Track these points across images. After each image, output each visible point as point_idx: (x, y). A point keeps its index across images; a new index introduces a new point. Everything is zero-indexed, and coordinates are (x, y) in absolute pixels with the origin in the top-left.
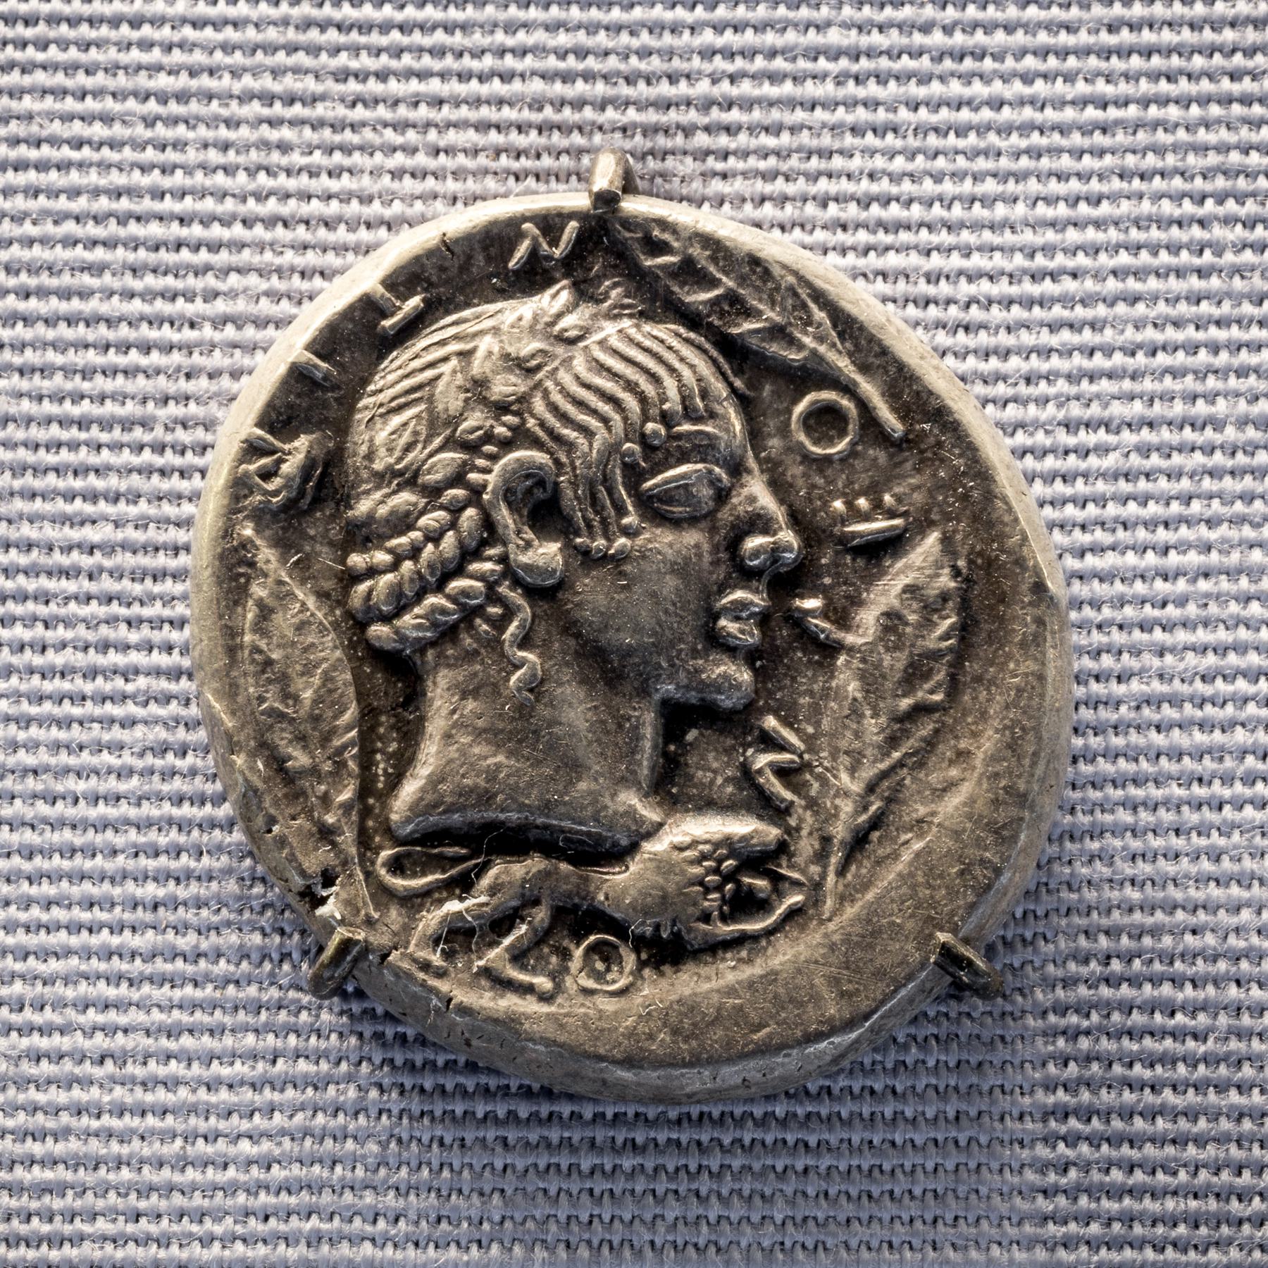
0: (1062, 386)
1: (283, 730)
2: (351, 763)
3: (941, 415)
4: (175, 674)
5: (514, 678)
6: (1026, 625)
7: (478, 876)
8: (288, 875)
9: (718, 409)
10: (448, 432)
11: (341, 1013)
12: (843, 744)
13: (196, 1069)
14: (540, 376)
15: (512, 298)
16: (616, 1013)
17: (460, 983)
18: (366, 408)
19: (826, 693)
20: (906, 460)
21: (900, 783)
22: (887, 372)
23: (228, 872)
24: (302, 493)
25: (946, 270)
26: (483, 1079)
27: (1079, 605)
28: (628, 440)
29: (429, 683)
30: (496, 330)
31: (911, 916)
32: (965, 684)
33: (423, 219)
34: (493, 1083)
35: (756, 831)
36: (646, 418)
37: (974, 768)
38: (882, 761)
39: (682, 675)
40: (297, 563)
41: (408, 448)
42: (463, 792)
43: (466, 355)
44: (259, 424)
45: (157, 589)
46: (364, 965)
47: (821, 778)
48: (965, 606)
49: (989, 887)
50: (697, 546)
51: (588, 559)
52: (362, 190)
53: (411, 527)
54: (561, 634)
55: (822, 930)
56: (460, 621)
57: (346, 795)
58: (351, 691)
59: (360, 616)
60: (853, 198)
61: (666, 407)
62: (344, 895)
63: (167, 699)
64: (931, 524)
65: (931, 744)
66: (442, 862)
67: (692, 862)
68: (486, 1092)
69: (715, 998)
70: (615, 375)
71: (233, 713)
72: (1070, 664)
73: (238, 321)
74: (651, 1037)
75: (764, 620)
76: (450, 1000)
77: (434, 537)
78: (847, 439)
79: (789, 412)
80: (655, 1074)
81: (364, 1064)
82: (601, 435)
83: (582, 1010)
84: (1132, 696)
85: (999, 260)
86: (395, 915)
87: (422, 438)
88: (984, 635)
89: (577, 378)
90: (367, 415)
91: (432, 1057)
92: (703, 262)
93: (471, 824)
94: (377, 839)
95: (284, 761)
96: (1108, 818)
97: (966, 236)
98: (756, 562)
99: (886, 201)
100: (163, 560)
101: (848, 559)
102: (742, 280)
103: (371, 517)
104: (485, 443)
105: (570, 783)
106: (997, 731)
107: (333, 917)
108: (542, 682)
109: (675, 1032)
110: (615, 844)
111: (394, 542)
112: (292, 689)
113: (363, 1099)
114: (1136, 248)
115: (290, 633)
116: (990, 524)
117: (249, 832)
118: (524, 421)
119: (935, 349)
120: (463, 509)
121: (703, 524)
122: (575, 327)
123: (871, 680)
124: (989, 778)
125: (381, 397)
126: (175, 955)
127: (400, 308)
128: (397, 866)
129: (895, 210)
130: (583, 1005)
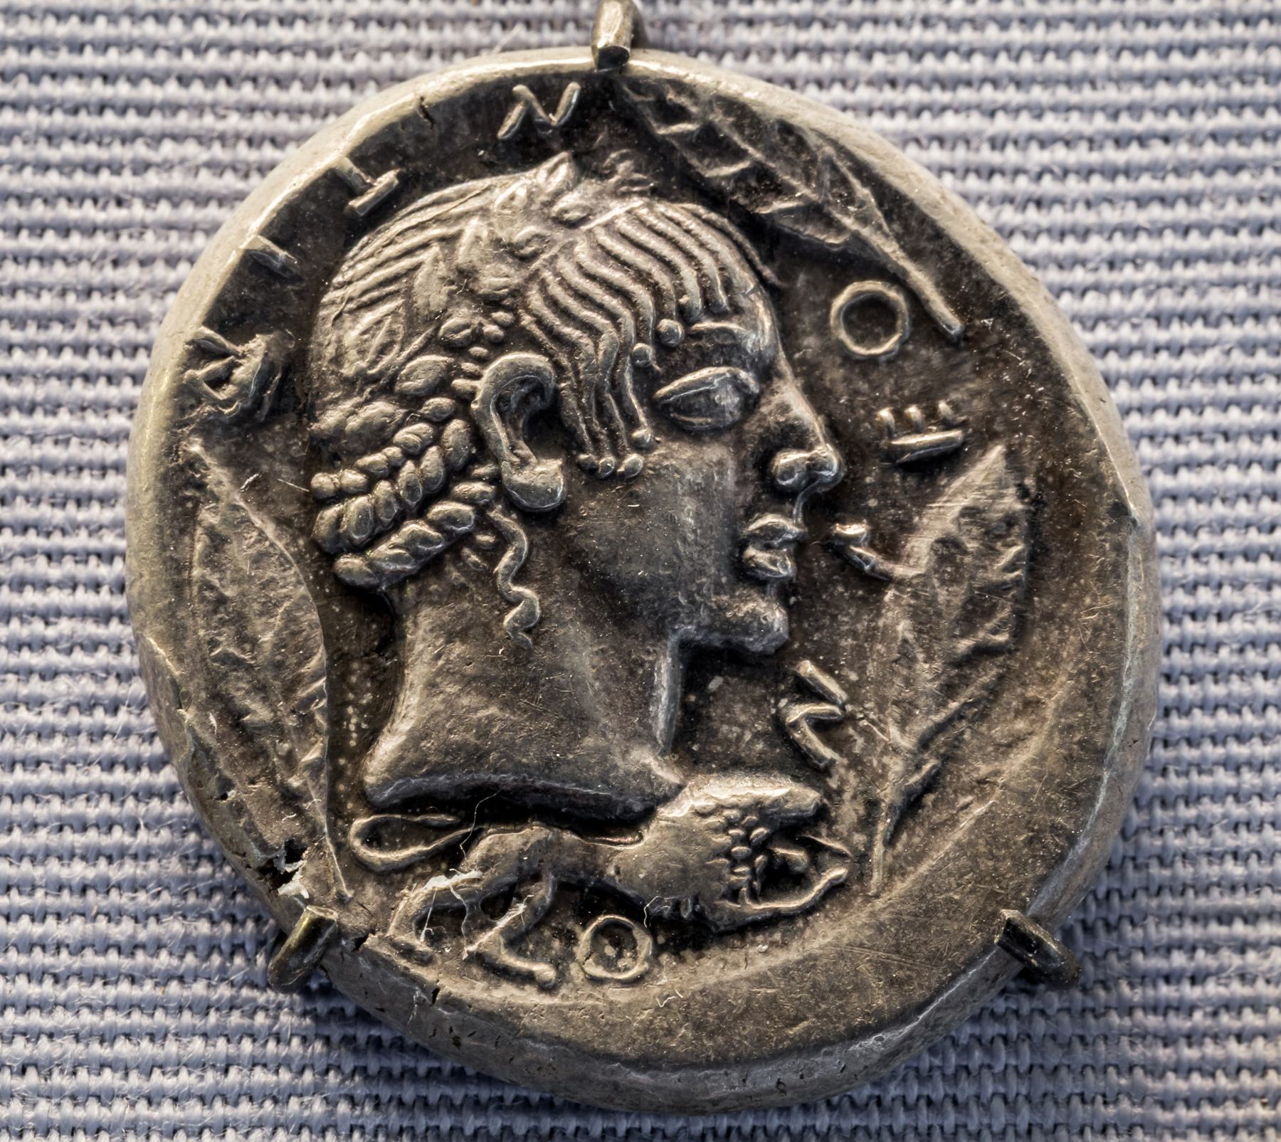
0: (1151, 271)
1: (239, 679)
2: (318, 718)
3: (1005, 309)
4: (104, 616)
5: (508, 617)
6: (1104, 554)
7: (468, 847)
8: (245, 847)
9: (744, 303)
10: (429, 331)
11: (304, 1014)
12: (892, 693)
13: (135, 1079)
14: (536, 265)
15: (502, 172)
16: (629, 1005)
17: (449, 972)
18: (333, 303)
19: (872, 635)
20: (964, 361)
21: (959, 738)
22: (941, 258)
23: (168, 849)
24: (258, 403)
25: (1014, 134)
26: (473, 1091)
27: (1170, 529)
28: (640, 339)
29: (409, 624)
30: (484, 212)
31: (972, 891)
32: (1033, 622)
33: (396, 78)
34: (485, 1094)
35: (790, 794)
36: (661, 314)
37: (1044, 719)
38: (937, 712)
39: (703, 613)
40: (252, 485)
41: (383, 350)
42: (449, 750)
43: (449, 241)
44: (208, 322)
45: (82, 515)
46: (336, 952)
47: (865, 732)
48: (1033, 532)
49: (1062, 858)
50: (720, 463)
51: (593, 478)
52: (319, 41)
53: (387, 442)
54: (563, 565)
55: (868, 908)
56: (446, 550)
57: (313, 755)
58: (318, 633)
59: (327, 546)
60: (902, 48)
61: (683, 300)
62: (312, 871)
63: (92, 646)
64: (994, 436)
65: (994, 692)
66: (426, 832)
67: (716, 830)
68: (478, 1106)
69: (745, 987)
70: (624, 264)
71: (180, 660)
72: (1157, 598)
73: (175, 198)
74: (670, 1032)
75: (799, 548)
76: (437, 991)
77: (417, 454)
78: (895, 338)
79: (827, 305)
80: (676, 1076)
81: (332, 1074)
82: (609, 334)
83: (590, 1002)
84: (1233, 637)
85: (1076, 123)
86: (371, 893)
87: (399, 338)
88: (1055, 565)
89: (580, 267)
90: (334, 311)
91: (412, 1064)
92: (726, 131)
93: (459, 787)
94: (350, 806)
95: (241, 715)
96: (1206, 781)
97: (1038, 94)
98: (789, 482)
99: (942, 52)
100: (87, 482)
101: (897, 477)
102: (772, 151)
103: (339, 429)
104: (472, 344)
105: (575, 739)
106: (1071, 677)
107: (300, 896)
108: (542, 620)
109: (698, 1026)
110: (627, 810)
111: (367, 460)
112: (249, 632)
113: (332, 1113)
114: (1237, 107)
115: (246, 567)
116: (1063, 436)
117: (202, 803)
118: (518, 318)
119: (999, 230)
120: (448, 420)
121: (728, 437)
122: (577, 207)
123: (924, 617)
124: (1061, 732)
125: (350, 291)
126: (105, 946)
127: (371, 186)
128: (373, 837)
129: (953, 63)
130: (590, 996)
